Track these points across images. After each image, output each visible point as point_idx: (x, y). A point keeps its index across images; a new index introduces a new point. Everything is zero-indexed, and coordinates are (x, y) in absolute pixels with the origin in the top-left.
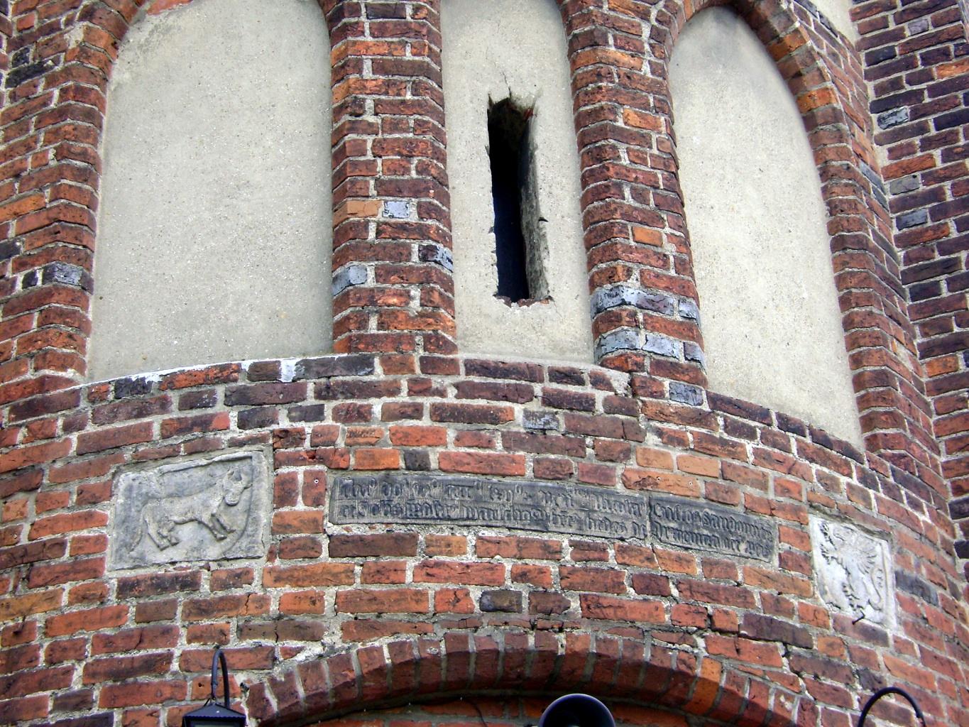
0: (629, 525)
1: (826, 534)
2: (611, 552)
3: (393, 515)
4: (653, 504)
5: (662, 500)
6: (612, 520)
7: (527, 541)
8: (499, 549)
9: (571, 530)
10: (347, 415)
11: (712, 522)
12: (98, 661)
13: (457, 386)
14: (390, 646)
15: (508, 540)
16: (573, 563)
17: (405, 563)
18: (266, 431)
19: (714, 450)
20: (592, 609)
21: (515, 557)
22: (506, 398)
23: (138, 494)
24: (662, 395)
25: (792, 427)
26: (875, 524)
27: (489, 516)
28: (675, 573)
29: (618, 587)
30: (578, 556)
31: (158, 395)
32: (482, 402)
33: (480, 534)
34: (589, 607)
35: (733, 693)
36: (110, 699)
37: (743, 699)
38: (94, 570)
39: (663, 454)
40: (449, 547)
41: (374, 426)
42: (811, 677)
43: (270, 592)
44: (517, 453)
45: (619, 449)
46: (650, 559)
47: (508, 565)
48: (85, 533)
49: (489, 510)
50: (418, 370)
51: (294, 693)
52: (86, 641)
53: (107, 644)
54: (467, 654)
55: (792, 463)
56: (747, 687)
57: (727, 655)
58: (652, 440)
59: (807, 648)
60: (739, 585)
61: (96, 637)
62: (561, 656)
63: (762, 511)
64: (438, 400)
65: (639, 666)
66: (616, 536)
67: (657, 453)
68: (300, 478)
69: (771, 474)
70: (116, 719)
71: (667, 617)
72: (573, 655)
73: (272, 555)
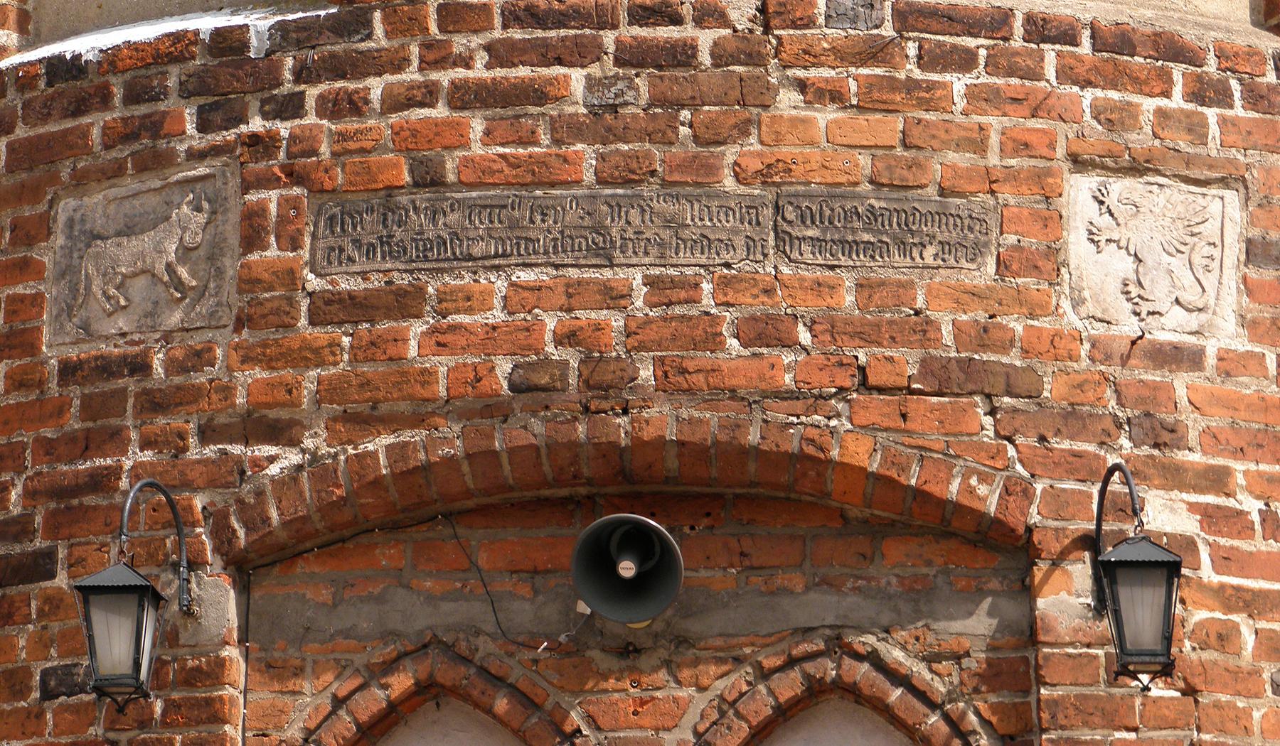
0: (740, 242)
1: (1102, 203)
2: (707, 287)
3: (392, 257)
4: (781, 203)
5: (796, 195)
6: (712, 237)
7: (579, 282)
8: (539, 299)
9: (647, 260)
10: (334, 107)
11: (882, 217)
12: (39, 474)
13: (488, 48)
14: (389, 448)
15: (551, 283)
16: (647, 310)
17: (407, 328)
18: (230, 135)
19: (893, 102)
20: (673, 382)
21: (561, 309)
22: (560, 61)
23: (81, 232)
24: (810, 23)
25: (1054, 33)
26: (1211, 167)
27: (526, 248)
28: (808, 306)
29: (714, 341)
30: (655, 299)
31: (98, 81)
32: (523, 72)
33: (514, 279)
34: (666, 373)
35: (890, 481)
36: (54, 527)
37: (909, 486)
38: (31, 347)
39: (804, 121)
40: (470, 301)
41: (371, 122)
42: (1033, 441)
43: (236, 378)
44: (573, 148)
45: (733, 121)
46: (768, 292)
47: (551, 322)
48: (19, 289)
49: (528, 239)
50: (433, 28)
51: (266, 520)
52: (24, 446)
53: (48, 449)
54: (495, 454)
55: (1041, 97)
56: (915, 468)
57: (885, 425)
58: (788, 100)
59: (1030, 397)
60: (917, 313)
61: (36, 440)
62: (627, 446)
63: (973, 188)
64: (460, 73)
65: (747, 452)
66: (718, 261)
67: (795, 121)
68: (273, 208)
69: (994, 122)
70: (60, 556)
71: (788, 379)
72: (638, 444)
73: (239, 325)
